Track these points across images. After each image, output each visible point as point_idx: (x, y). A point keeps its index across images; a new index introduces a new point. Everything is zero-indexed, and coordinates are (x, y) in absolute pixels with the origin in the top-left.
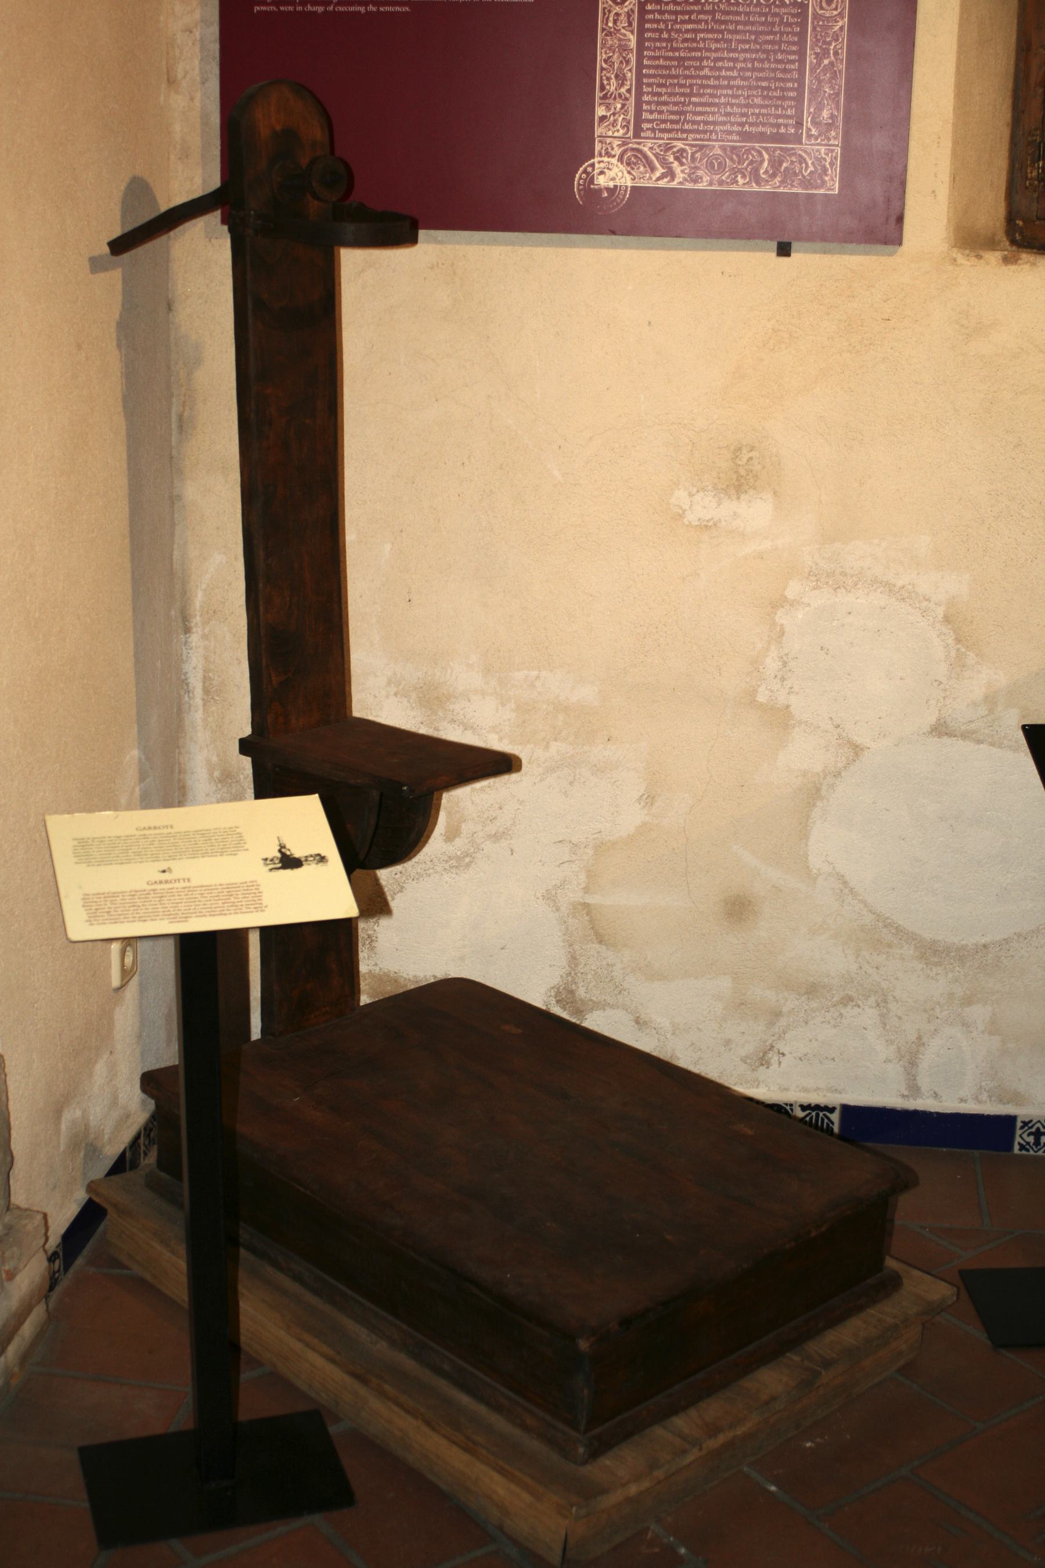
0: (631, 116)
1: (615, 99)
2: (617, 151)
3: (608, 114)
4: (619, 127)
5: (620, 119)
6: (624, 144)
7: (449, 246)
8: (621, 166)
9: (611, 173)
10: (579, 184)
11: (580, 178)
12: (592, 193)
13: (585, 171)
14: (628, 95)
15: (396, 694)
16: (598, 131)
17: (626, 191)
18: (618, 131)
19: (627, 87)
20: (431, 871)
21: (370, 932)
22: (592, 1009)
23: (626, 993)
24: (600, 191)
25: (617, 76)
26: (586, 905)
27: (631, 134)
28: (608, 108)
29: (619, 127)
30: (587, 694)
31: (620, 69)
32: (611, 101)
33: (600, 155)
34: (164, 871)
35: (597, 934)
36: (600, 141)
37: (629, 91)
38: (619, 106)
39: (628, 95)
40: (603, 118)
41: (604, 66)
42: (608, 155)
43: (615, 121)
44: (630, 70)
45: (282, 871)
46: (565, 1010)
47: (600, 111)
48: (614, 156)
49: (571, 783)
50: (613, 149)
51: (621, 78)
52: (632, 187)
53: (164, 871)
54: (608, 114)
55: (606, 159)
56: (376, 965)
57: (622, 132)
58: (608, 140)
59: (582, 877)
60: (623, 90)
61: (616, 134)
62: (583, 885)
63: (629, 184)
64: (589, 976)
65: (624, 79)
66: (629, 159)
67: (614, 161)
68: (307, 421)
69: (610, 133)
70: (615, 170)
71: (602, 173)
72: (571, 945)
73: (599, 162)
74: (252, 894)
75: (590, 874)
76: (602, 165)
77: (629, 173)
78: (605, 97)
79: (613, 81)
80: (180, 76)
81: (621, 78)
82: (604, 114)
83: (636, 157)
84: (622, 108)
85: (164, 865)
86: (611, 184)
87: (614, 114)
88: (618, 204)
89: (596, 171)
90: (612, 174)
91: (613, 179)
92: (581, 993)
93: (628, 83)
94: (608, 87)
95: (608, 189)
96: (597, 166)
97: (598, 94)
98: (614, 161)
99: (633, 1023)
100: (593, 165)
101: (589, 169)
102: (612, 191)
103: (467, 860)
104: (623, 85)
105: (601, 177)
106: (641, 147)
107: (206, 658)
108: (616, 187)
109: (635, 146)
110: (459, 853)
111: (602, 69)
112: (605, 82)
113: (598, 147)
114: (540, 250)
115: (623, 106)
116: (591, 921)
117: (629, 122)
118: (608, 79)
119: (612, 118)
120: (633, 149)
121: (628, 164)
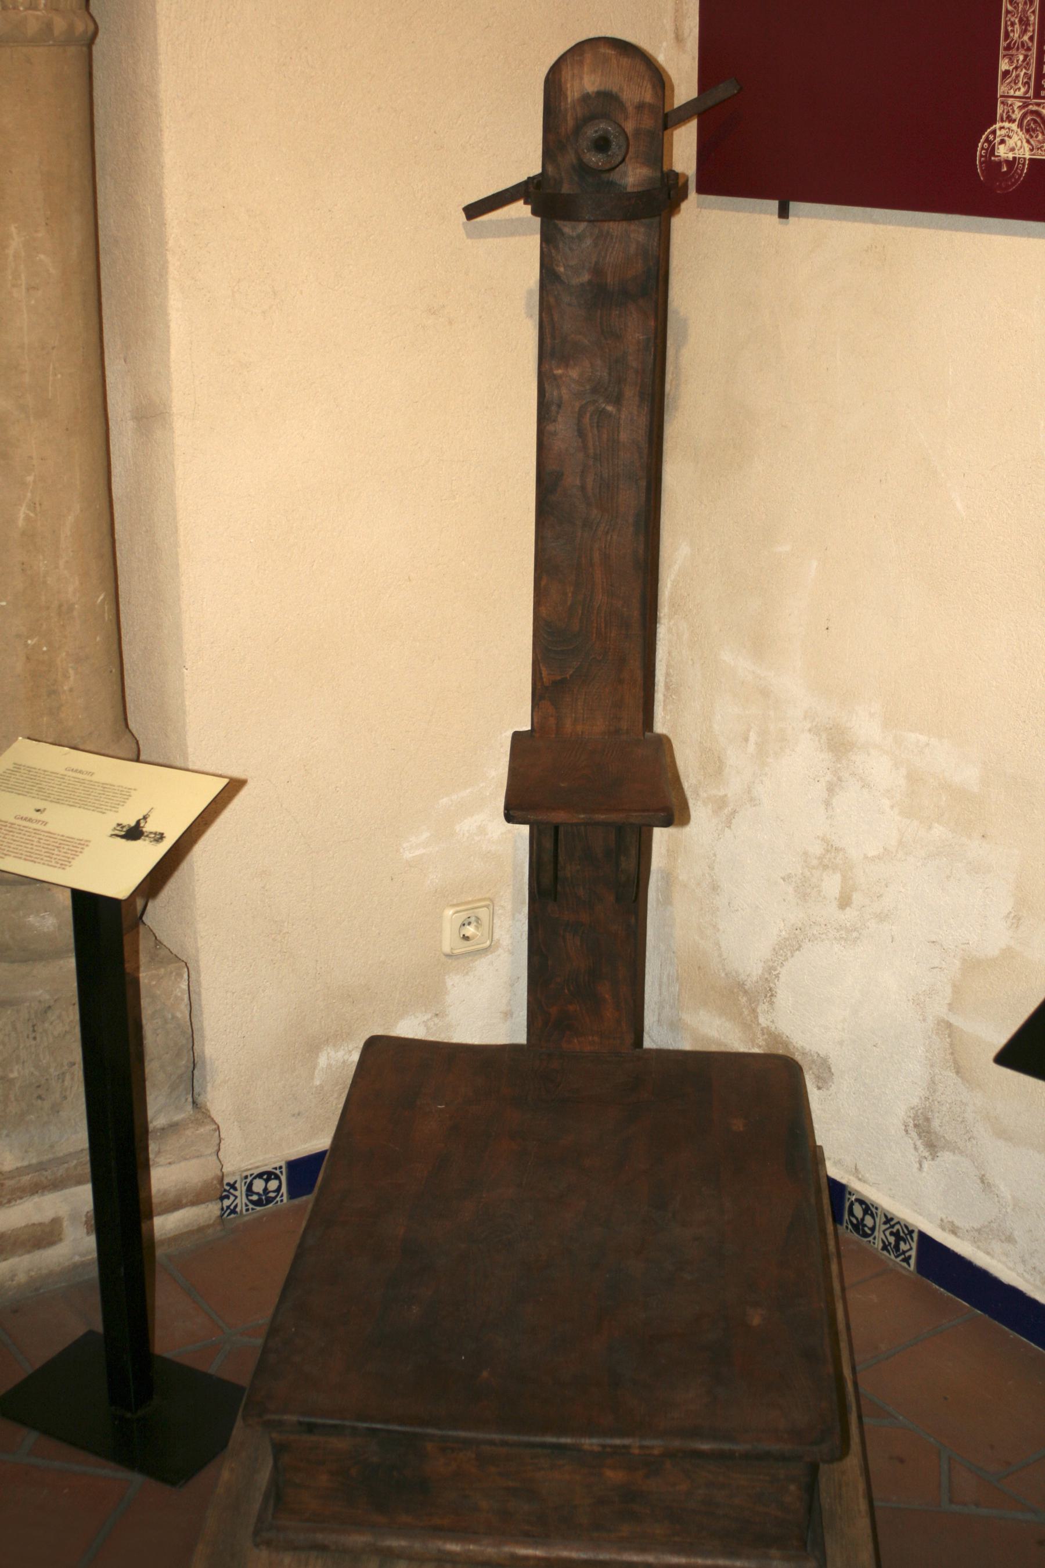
0: (1032, 71)
1: (1018, 49)
2: (1017, 115)
3: (1011, 68)
4: (1020, 85)
5: (1022, 74)
6: (1025, 105)
7: (882, 227)
8: (1021, 133)
9: (1012, 144)
10: (981, 156)
11: (983, 148)
12: (993, 166)
13: (987, 140)
14: (1030, 44)
15: (810, 730)
16: (1002, 89)
17: (1024, 164)
18: (1019, 89)
19: (1030, 34)
20: (824, 936)
21: (772, 985)
22: (944, 1148)
23: (974, 1142)
24: (999, 164)
25: (1021, 21)
26: (949, 1025)
27: (1031, 93)
28: (1011, 62)
29: (1020, 85)
30: (969, 776)
31: (1024, 11)
32: (1014, 52)
33: (1002, 121)
34: (38, 811)
35: (955, 1062)
36: (1002, 103)
37: (1031, 38)
38: (1021, 58)
39: (1030, 44)
40: (1006, 73)
41: (1010, 8)
42: (1011, 120)
43: (1017, 76)
44: (1033, 12)
45: (123, 841)
46: (920, 1138)
47: (1004, 65)
48: (1014, 121)
49: (948, 877)
50: (1013, 112)
51: (1024, 22)
52: (1030, 159)
53: (38, 811)
54: (1011, 68)
55: (1006, 124)
56: (773, 1022)
57: (1023, 90)
58: (1010, 101)
59: (949, 990)
60: (1026, 38)
61: (1018, 94)
62: (947, 1001)
63: (1028, 156)
64: (944, 1109)
65: (1027, 24)
66: (1028, 124)
67: (1014, 126)
68: (610, 408)
69: (1012, 93)
70: (1015, 138)
71: (1002, 142)
72: (932, 1066)
73: (1001, 128)
74: (70, 848)
75: (956, 989)
76: (1003, 132)
77: (1028, 142)
78: (1008, 48)
79: (1017, 26)
80: (686, 35)
81: (1024, 22)
82: (1007, 67)
83: (1035, 122)
84: (1024, 61)
85: (40, 805)
86: (1010, 156)
87: (1016, 68)
88: (1017, 180)
89: (998, 140)
90: (1010, 143)
91: (1012, 150)
92: (936, 1124)
93: (1031, 29)
94: (1011, 35)
95: (1007, 162)
96: (998, 133)
97: (1003, 44)
98: (1014, 126)
99: (979, 1181)
100: (994, 132)
101: (991, 137)
102: (1011, 163)
103: (855, 934)
104: (1025, 31)
105: (1002, 147)
106: (1040, 109)
107: (669, 653)
108: (1014, 158)
109: (1035, 108)
110: (848, 924)
111: (1008, 12)
112: (1010, 29)
113: (1000, 109)
114: (959, 235)
115: (1026, 57)
116: (951, 1044)
117: (1030, 78)
118: (1013, 24)
119: (1014, 74)
120: (1032, 112)
121: (1028, 131)
